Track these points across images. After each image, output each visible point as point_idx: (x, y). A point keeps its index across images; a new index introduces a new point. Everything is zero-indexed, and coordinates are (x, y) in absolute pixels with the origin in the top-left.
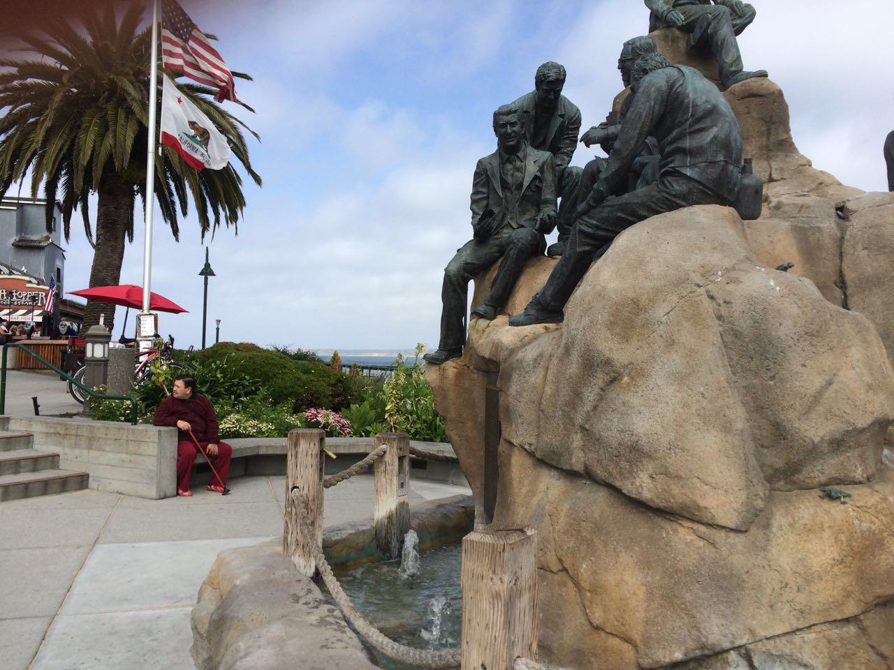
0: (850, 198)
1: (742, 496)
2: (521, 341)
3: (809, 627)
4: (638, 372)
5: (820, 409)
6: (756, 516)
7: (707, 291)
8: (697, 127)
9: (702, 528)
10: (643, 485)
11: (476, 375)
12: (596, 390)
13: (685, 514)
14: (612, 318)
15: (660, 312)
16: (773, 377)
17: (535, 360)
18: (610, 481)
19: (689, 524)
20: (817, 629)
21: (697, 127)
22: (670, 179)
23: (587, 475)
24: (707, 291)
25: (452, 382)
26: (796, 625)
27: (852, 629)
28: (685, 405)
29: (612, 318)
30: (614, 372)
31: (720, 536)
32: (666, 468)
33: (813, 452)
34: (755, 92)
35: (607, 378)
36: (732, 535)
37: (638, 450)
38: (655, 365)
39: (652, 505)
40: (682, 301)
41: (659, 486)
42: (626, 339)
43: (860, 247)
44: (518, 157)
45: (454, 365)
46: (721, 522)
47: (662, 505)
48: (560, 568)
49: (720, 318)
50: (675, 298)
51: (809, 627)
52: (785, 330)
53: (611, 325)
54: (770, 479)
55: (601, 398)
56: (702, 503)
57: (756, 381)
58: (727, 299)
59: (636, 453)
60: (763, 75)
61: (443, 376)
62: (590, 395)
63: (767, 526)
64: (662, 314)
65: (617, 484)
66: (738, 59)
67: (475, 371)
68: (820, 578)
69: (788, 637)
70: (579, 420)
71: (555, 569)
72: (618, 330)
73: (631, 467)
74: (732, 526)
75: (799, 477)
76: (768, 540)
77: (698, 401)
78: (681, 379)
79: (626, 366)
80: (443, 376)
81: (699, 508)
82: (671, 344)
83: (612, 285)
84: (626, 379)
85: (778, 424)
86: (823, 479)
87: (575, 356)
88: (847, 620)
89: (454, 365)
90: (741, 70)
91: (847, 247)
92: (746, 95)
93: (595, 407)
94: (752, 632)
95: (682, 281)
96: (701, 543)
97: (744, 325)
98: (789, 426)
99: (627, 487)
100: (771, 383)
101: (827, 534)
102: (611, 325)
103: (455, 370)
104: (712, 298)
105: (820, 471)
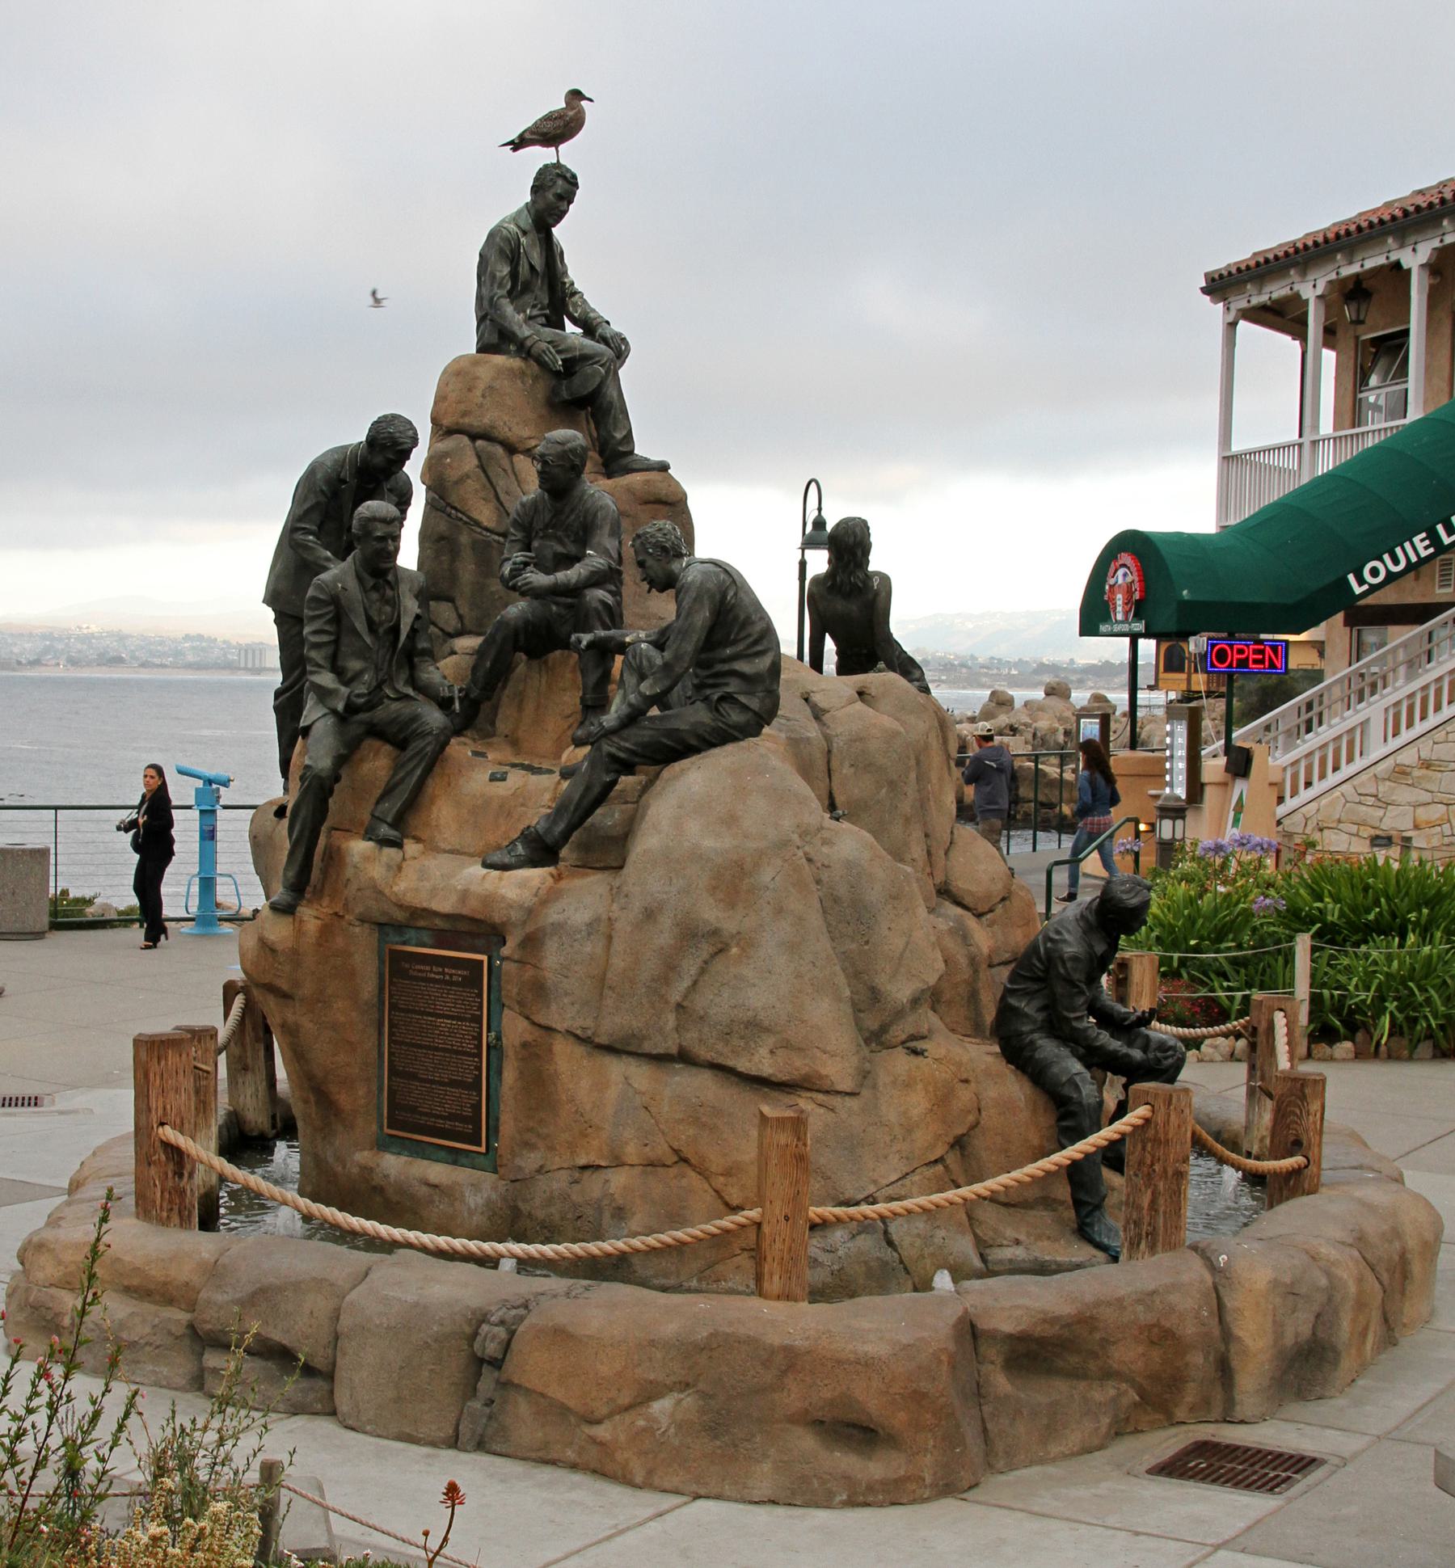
0: (814, 689)
1: (855, 1060)
2: (536, 895)
3: (913, 1171)
4: (747, 943)
5: (902, 970)
6: (865, 1077)
7: (806, 854)
8: (759, 648)
9: (820, 1097)
10: (762, 1062)
11: (357, 930)
12: (699, 961)
13: (806, 1085)
14: (713, 882)
15: (766, 875)
16: (867, 943)
17: (590, 925)
18: (721, 1060)
19: (809, 1094)
20: (918, 1171)
21: (759, 648)
22: (724, 705)
23: (684, 1057)
24: (806, 854)
25: (314, 940)
26: (905, 1170)
27: (940, 1168)
28: (799, 976)
29: (713, 882)
30: (721, 942)
31: (836, 1101)
32: (788, 1041)
33: (899, 1014)
34: (664, 499)
35: (712, 950)
36: (847, 1098)
37: (756, 1025)
38: (765, 934)
39: (773, 1079)
40: (786, 865)
41: (779, 1060)
42: (732, 906)
43: (847, 764)
44: (388, 583)
45: (315, 913)
46: (839, 1088)
47: (785, 1078)
48: (676, 1159)
49: (818, 882)
50: (779, 862)
51: (913, 1171)
52: (874, 895)
53: (713, 890)
54: (867, 1041)
55: (703, 971)
56: (824, 1072)
57: (854, 946)
58: (826, 863)
59: (754, 1027)
60: (663, 467)
61: (299, 932)
62: (690, 966)
63: (874, 1087)
64: (769, 879)
65: (730, 1063)
66: (629, 438)
67: (357, 923)
68: (918, 1126)
69: (900, 1183)
70: (675, 997)
71: (669, 1163)
72: (721, 896)
73: (747, 1043)
74: (848, 1090)
75: (886, 1037)
76: (877, 1099)
77: (810, 970)
78: (792, 948)
79: (732, 937)
80: (299, 932)
81: (821, 1077)
82: (779, 911)
83: (709, 843)
84: (734, 950)
85: (873, 988)
86: (903, 1037)
87: (666, 921)
88: (936, 1161)
89: (315, 913)
90: (632, 452)
91: (834, 764)
92: (652, 499)
93: (695, 983)
94: (875, 1182)
95: (784, 844)
96: (822, 1111)
97: (842, 890)
98: (883, 990)
99: (743, 1065)
100: (866, 947)
101: (920, 1086)
102: (713, 890)
103: (319, 922)
104: (809, 860)
105: (899, 1032)
